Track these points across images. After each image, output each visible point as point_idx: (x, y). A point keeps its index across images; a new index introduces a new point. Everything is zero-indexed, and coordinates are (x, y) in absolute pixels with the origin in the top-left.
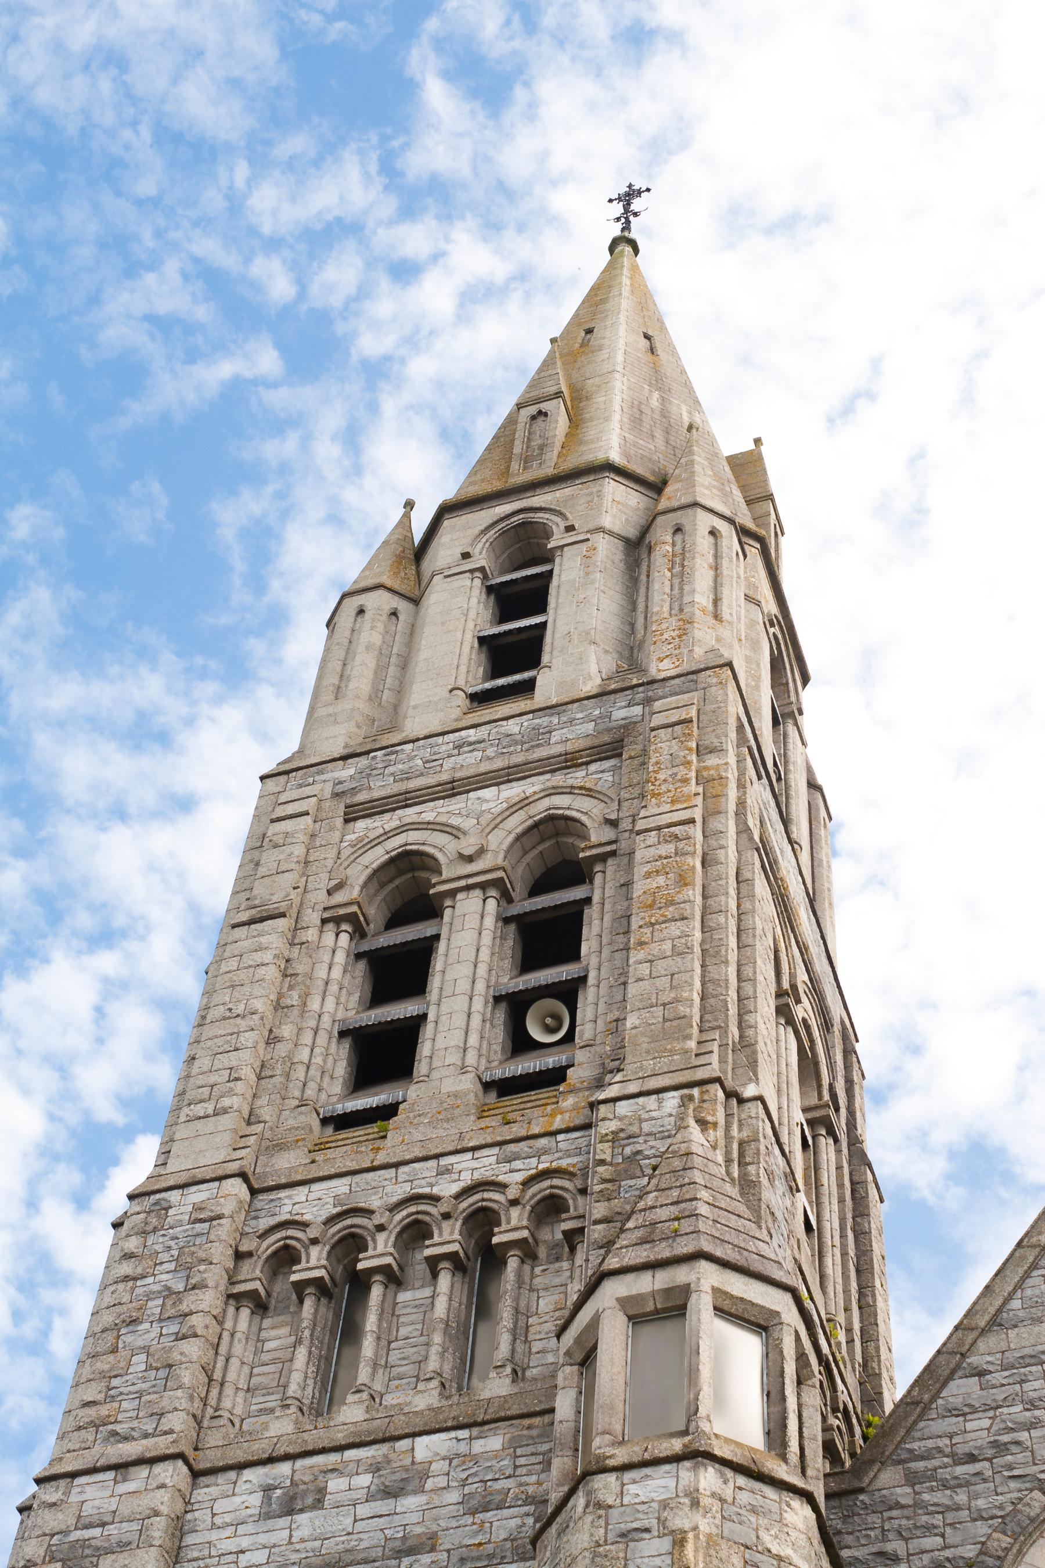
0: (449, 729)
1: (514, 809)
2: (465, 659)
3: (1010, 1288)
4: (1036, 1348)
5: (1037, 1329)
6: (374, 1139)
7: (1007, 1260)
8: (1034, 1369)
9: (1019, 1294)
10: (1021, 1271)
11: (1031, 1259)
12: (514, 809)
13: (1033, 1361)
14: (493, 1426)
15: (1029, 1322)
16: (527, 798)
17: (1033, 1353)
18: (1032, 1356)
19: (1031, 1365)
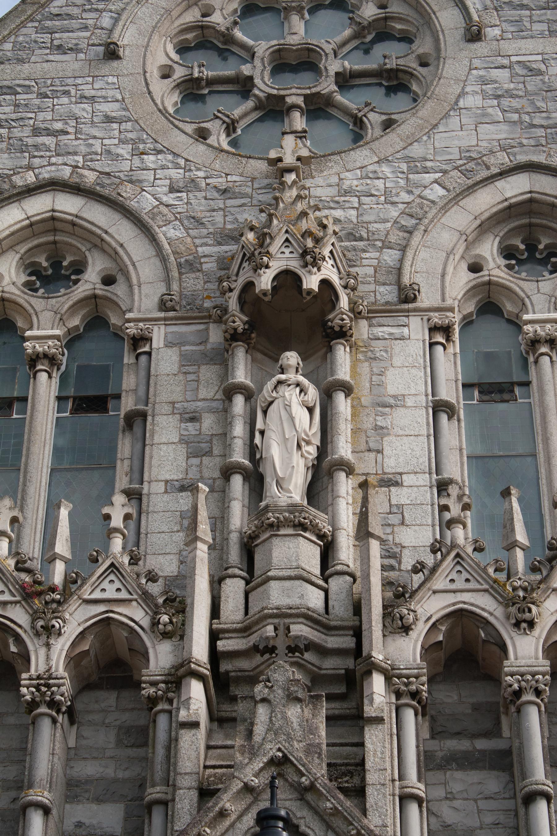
0: (250, 604)
1: (101, 579)
2: (51, 408)
3: (6, 33)
4: (14, 82)
5: (19, 67)
6: (147, 521)
7: (11, 12)
8: (8, 97)
9: (12, 39)
10: (18, 21)
11: (29, 13)
12: (101, 579)
13: (9, 91)
14: (151, 390)
15: (15, 61)
16: (434, 14)
17: (11, 85)
18: (9, 87)
19: (7, 94)
